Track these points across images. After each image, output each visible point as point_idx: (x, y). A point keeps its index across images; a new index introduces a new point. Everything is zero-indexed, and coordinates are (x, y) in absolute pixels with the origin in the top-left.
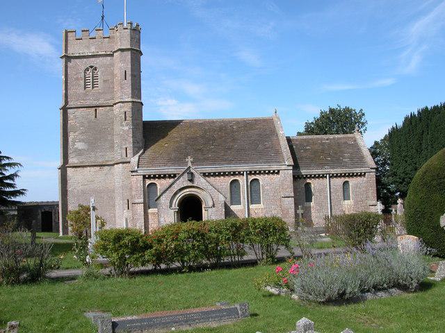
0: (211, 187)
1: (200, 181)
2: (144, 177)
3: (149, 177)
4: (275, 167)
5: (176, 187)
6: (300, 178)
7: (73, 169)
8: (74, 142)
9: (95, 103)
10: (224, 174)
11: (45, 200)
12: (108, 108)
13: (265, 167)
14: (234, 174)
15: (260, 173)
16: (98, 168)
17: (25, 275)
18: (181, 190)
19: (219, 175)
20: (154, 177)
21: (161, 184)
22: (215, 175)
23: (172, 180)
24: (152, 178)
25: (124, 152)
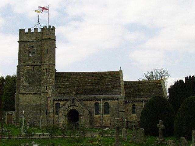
0: (82, 106)
1: (77, 103)
2: (54, 100)
3: (56, 100)
4: (116, 97)
5: (66, 106)
6: (130, 102)
7: (22, 95)
8: (23, 82)
9: (33, 64)
10: (92, 100)
11: (107, 71)
12: (39, 66)
13: (110, 96)
14: (96, 100)
15: (109, 99)
16: (33, 95)
17: (24, 112)
18: (69, 107)
19: (89, 100)
20: (59, 100)
21: (61, 103)
22: (87, 100)
23: (65, 102)
24: (58, 100)
25: (46, 88)
